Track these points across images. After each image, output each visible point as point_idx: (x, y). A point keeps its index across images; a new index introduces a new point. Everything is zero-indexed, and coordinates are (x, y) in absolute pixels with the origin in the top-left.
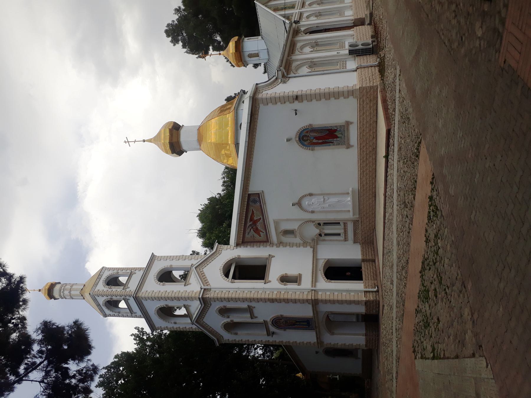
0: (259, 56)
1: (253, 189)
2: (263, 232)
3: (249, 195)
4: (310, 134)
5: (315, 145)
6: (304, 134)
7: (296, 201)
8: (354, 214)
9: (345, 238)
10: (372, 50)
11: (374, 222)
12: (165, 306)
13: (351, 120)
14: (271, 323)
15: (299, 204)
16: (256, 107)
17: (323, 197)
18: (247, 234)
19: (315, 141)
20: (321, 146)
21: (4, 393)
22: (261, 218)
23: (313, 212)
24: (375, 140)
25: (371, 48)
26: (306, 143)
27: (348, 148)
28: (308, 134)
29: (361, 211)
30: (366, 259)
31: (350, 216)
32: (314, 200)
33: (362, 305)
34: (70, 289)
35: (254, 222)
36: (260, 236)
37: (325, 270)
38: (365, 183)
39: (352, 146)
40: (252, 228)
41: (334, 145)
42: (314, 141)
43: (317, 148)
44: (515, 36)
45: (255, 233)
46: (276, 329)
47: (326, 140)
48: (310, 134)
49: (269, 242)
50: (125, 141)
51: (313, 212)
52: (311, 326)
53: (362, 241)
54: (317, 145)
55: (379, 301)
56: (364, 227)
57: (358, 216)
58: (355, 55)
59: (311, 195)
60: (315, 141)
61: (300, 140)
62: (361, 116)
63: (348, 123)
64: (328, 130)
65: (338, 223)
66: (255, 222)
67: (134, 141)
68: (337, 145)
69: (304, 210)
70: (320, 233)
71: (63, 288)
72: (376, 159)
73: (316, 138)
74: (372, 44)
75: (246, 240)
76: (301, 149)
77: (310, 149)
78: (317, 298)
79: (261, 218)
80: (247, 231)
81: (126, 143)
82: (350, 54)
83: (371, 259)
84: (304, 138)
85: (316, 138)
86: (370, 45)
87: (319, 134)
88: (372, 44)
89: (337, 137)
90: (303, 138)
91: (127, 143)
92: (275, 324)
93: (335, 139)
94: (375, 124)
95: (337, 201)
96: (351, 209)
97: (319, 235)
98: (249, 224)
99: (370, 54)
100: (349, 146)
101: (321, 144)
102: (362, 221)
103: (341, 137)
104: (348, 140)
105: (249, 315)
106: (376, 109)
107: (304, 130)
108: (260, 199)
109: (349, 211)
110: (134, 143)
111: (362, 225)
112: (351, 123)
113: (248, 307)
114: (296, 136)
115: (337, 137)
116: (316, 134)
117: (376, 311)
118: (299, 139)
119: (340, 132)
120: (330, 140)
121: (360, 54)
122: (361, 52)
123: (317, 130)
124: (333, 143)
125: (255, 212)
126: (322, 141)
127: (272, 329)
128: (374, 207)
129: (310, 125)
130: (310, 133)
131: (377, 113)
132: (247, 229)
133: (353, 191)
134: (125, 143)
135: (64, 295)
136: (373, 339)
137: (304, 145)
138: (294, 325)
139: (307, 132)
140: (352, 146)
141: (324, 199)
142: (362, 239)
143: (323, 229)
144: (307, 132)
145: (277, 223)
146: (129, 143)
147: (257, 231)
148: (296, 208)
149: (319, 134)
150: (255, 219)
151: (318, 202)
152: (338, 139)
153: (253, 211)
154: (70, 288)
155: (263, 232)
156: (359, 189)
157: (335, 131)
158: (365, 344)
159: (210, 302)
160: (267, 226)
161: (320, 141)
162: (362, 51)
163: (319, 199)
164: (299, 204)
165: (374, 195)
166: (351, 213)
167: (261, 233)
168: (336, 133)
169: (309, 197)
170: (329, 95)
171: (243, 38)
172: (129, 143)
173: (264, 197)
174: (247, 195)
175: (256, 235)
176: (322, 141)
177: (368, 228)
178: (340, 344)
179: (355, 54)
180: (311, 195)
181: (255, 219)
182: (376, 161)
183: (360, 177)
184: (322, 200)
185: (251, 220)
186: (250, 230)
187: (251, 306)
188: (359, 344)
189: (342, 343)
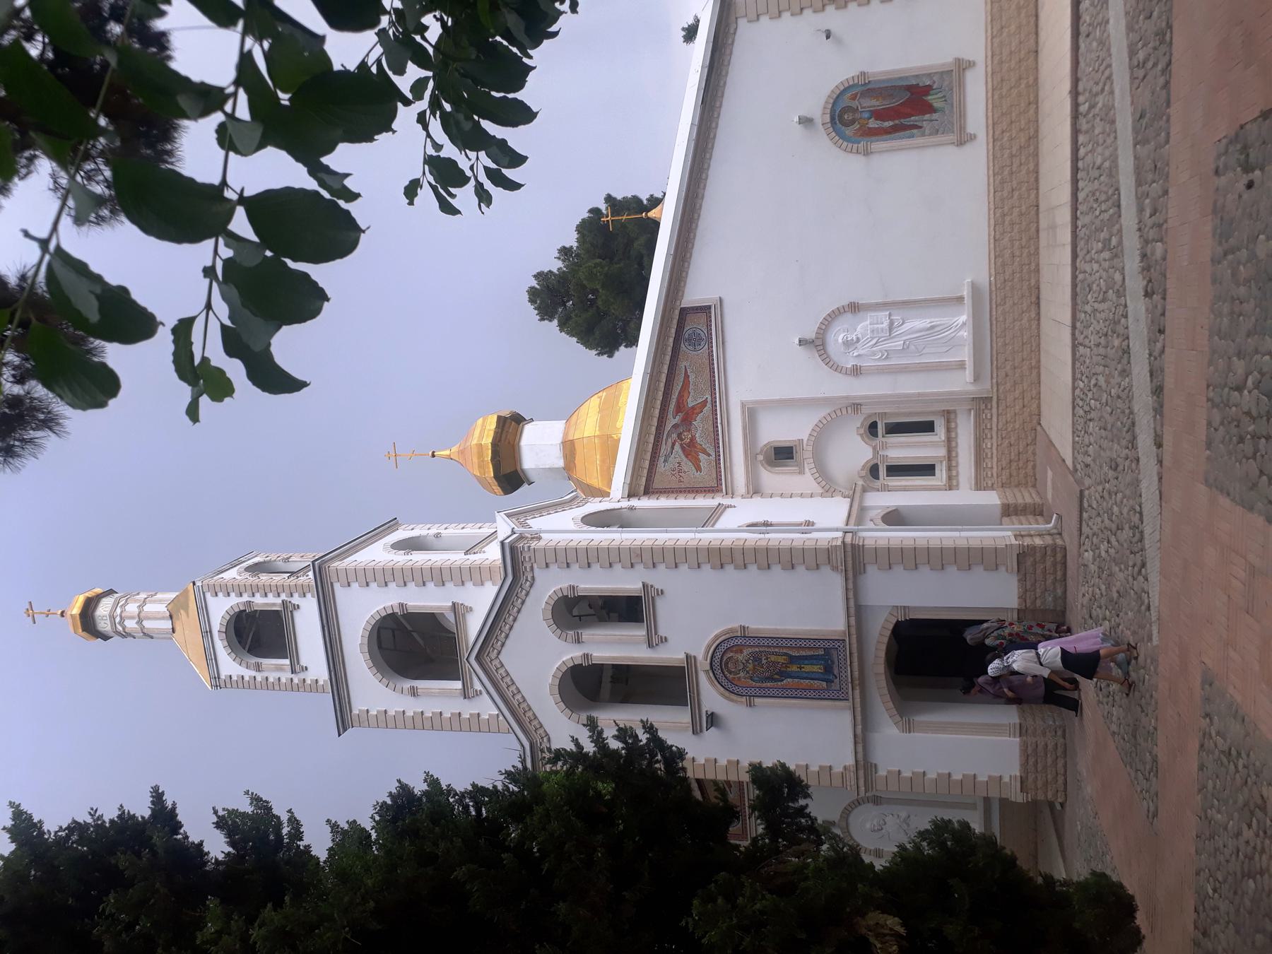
1: (694, 295)
2: (709, 455)
3: (684, 312)
4: (860, 103)
5: (873, 138)
6: (846, 101)
7: (810, 334)
8: (977, 378)
9: (950, 478)
11: (1035, 106)
12: (397, 610)
13: (967, 56)
14: (708, 668)
15: (816, 343)
16: (728, 25)
17: (890, 315)
18: (662, 459)
19: (873, 124)
20: (890, 139)
22: (706, 401)
23: (856, 371)
24: (1035, 372)
26: (849, 131)
27: (961, 143)
28: (855, 104)
29: (997, 361)
30: (1016, 506)
31: (962, 383)
32: (864, 326)
33: (1007, 570)
34: (139, 615)
35: (687, 413)
36: (698, 469)
38: (1007, 253)
39: (973, 138)
40: (679, 436)
41: (923, 135)
42: (871, 125)
43: (878, 145)
45: (687, 457)
46: (722, 695)
47: (902, 120)
48: (860, 103)
49: (722, 490)
51: (856, 371)
52: (837, 681)
53: (1000, 479)
54: (879, 138)
55: (1065, 549)
56: (1007, 422)
57: (988, 386)
59: (854, 308)
60: (873, 124)
61: (835, 123)
62: (997, 139)
63: (962, 66)
64: (909, 88)
65: (928, 427)
66: (688, 417)
68: (930, 135)
69: (831, 363)
70: (875, 461)
71: (119, 611)
72: (1037, 172)
73: (878, 115)
75: (657, 484)
76: (835, 150)
77: (859, 151)
78: (861, 544)
79: (706, 401)
80: (664, 449)
83: (1030, 504)
84: (846, 117)
85: (878, 115)
87: (884, 103)
89: (930, 109)
90: (841, 116)
92: (718, 672)
93: (927, 117)
94: (1032, 58)
95: (929, 325)
96: (966, 355)
98: (672, 421)
100: (964, 139)
101: (890, 133)
102: (1002, 396)
103: (942, 110)
104: (962, 115)
105: (644, 633)
106: (1034, 13)
107: (845, 90)
108: (711, 330)
109: (961, 365)
111: (1000, 412)
112: (971, 64)
113: (644, 585)
114: (825, 108)
115: (930, 109)
116: (878, 103)
117: (1055, 599)
118: (832, 118)
119: (940, 95)
120: (913, 118)
123: (879, 88)
124: (921, 127)
125: (692, 378)
126: (891, 123)
127: (711, 696)
128: (1034, 344)
129: (863, 74)
130: (861, 100)
131: (1037, 26)
132: (664, 442)
133: (975, 288)
135: (123, 615)
136: (1046, 745)
137: (843, 137)
138: (784, 675)
139: (854, 98)
140: (973, 138)
141: (891, 323)
142: (1000, 468)
143: (884, 447)
144: (854, 98)
145: (751, 414)
147: (691, 450)
148: (807, 360)
149: (884, 103)
150: (691, 403)
151: (873, 331)
152: (935, 116)
153: (687, 376)
154: (137, 610)
155: (709, 455)
156: (990, 280)
157: (927, 90)
158: (1018, 774)
159: (532, 568)
160: (722, 424)
161: (887, 124)
163: (877, 324)
164: (816, 343)
165: (1034, 299)
166: (968, 374)
167: (702, 456)
168: (930, 97)
169: (849, 315)
173: (722, 322)
174: (677, 312)
175: (687, 466)
176: (891, 123)
177: (1017, 422)
178: (934, 776)
180: (854, 308)
181: (691, 403)
182: (1037, 180)
183: (994, 237)
184: (885, 324)
185: (679, 409)
186: (673, 444)
187: (652, 586)
188: (997, 774)
189: (940, 771)
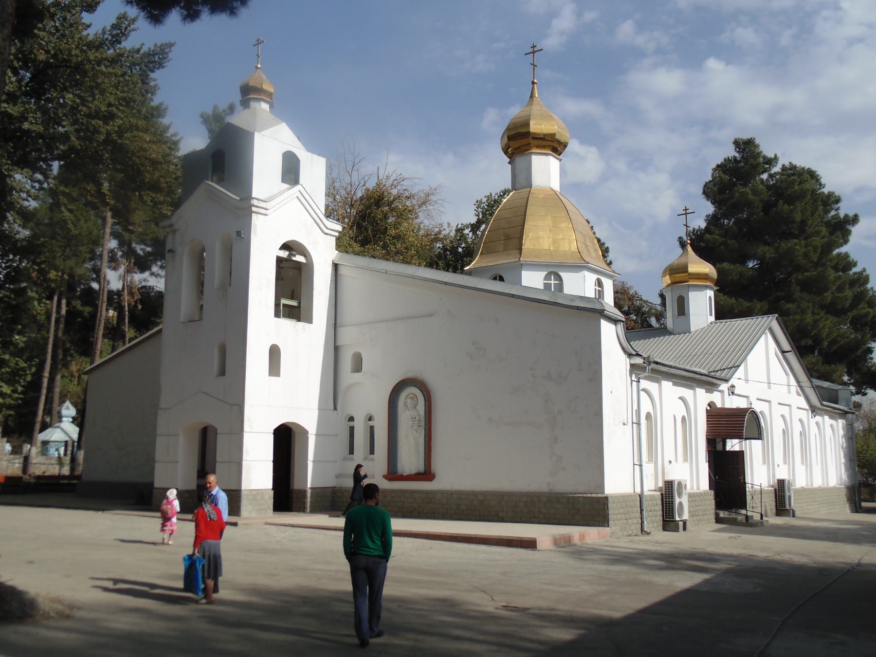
0: (679, 315)
10: (671, 519)
21: (228, 11)
25: (673, 518)
37: (286, 424)
44: (420, 317)
50: (536, 46)
58: (664, 490)
67: (688, 225)
74: (681, 521)
81: (532, 47)
82: (665, 482)
86: (679, 518)
88: (681, 521)
91: (684, 212)
97: (351, 417)
99: (663, 516)
110: (684, 225)
121: (664, 500)
122: (669, 499)
134: (532, 46)
146: (530, 53)
162: (669, 504)
170: (638, 503)
171: (713, 289)
172: (530, 53)
179: (666, 492)
